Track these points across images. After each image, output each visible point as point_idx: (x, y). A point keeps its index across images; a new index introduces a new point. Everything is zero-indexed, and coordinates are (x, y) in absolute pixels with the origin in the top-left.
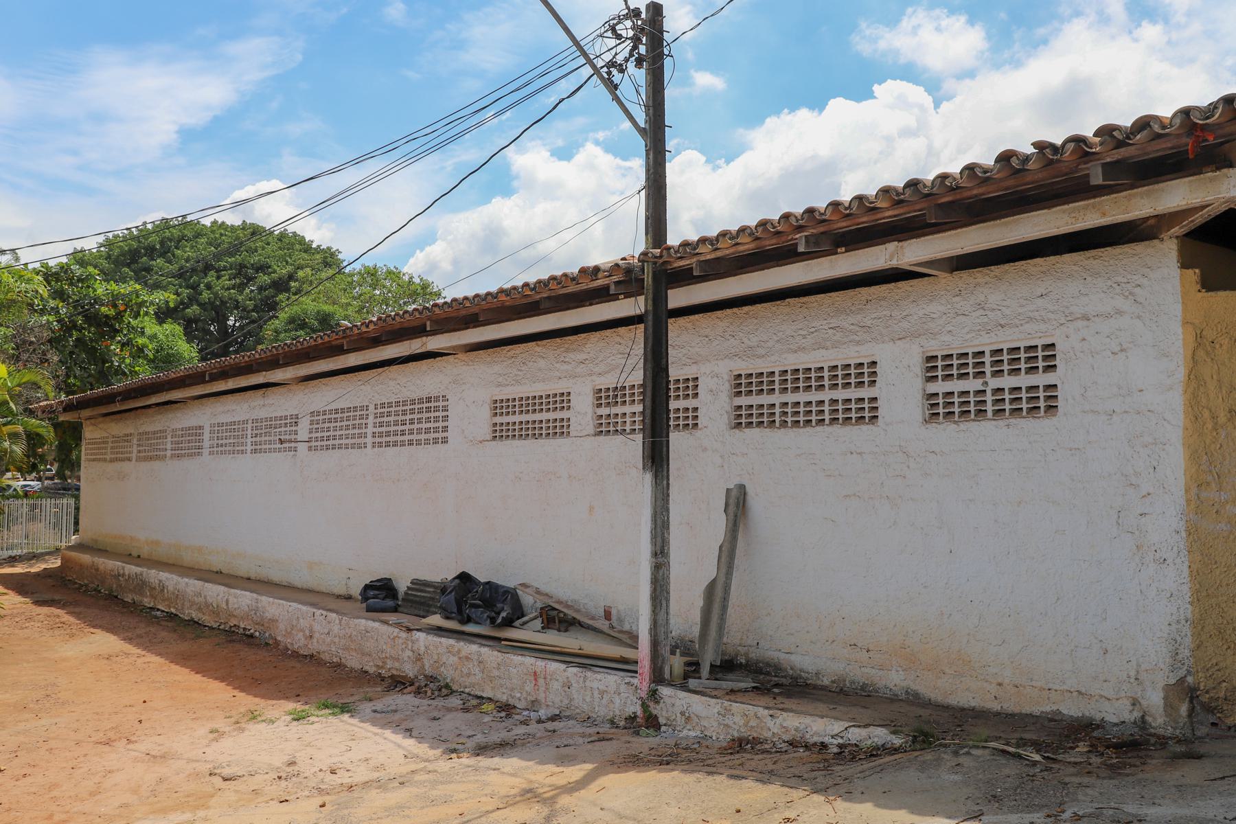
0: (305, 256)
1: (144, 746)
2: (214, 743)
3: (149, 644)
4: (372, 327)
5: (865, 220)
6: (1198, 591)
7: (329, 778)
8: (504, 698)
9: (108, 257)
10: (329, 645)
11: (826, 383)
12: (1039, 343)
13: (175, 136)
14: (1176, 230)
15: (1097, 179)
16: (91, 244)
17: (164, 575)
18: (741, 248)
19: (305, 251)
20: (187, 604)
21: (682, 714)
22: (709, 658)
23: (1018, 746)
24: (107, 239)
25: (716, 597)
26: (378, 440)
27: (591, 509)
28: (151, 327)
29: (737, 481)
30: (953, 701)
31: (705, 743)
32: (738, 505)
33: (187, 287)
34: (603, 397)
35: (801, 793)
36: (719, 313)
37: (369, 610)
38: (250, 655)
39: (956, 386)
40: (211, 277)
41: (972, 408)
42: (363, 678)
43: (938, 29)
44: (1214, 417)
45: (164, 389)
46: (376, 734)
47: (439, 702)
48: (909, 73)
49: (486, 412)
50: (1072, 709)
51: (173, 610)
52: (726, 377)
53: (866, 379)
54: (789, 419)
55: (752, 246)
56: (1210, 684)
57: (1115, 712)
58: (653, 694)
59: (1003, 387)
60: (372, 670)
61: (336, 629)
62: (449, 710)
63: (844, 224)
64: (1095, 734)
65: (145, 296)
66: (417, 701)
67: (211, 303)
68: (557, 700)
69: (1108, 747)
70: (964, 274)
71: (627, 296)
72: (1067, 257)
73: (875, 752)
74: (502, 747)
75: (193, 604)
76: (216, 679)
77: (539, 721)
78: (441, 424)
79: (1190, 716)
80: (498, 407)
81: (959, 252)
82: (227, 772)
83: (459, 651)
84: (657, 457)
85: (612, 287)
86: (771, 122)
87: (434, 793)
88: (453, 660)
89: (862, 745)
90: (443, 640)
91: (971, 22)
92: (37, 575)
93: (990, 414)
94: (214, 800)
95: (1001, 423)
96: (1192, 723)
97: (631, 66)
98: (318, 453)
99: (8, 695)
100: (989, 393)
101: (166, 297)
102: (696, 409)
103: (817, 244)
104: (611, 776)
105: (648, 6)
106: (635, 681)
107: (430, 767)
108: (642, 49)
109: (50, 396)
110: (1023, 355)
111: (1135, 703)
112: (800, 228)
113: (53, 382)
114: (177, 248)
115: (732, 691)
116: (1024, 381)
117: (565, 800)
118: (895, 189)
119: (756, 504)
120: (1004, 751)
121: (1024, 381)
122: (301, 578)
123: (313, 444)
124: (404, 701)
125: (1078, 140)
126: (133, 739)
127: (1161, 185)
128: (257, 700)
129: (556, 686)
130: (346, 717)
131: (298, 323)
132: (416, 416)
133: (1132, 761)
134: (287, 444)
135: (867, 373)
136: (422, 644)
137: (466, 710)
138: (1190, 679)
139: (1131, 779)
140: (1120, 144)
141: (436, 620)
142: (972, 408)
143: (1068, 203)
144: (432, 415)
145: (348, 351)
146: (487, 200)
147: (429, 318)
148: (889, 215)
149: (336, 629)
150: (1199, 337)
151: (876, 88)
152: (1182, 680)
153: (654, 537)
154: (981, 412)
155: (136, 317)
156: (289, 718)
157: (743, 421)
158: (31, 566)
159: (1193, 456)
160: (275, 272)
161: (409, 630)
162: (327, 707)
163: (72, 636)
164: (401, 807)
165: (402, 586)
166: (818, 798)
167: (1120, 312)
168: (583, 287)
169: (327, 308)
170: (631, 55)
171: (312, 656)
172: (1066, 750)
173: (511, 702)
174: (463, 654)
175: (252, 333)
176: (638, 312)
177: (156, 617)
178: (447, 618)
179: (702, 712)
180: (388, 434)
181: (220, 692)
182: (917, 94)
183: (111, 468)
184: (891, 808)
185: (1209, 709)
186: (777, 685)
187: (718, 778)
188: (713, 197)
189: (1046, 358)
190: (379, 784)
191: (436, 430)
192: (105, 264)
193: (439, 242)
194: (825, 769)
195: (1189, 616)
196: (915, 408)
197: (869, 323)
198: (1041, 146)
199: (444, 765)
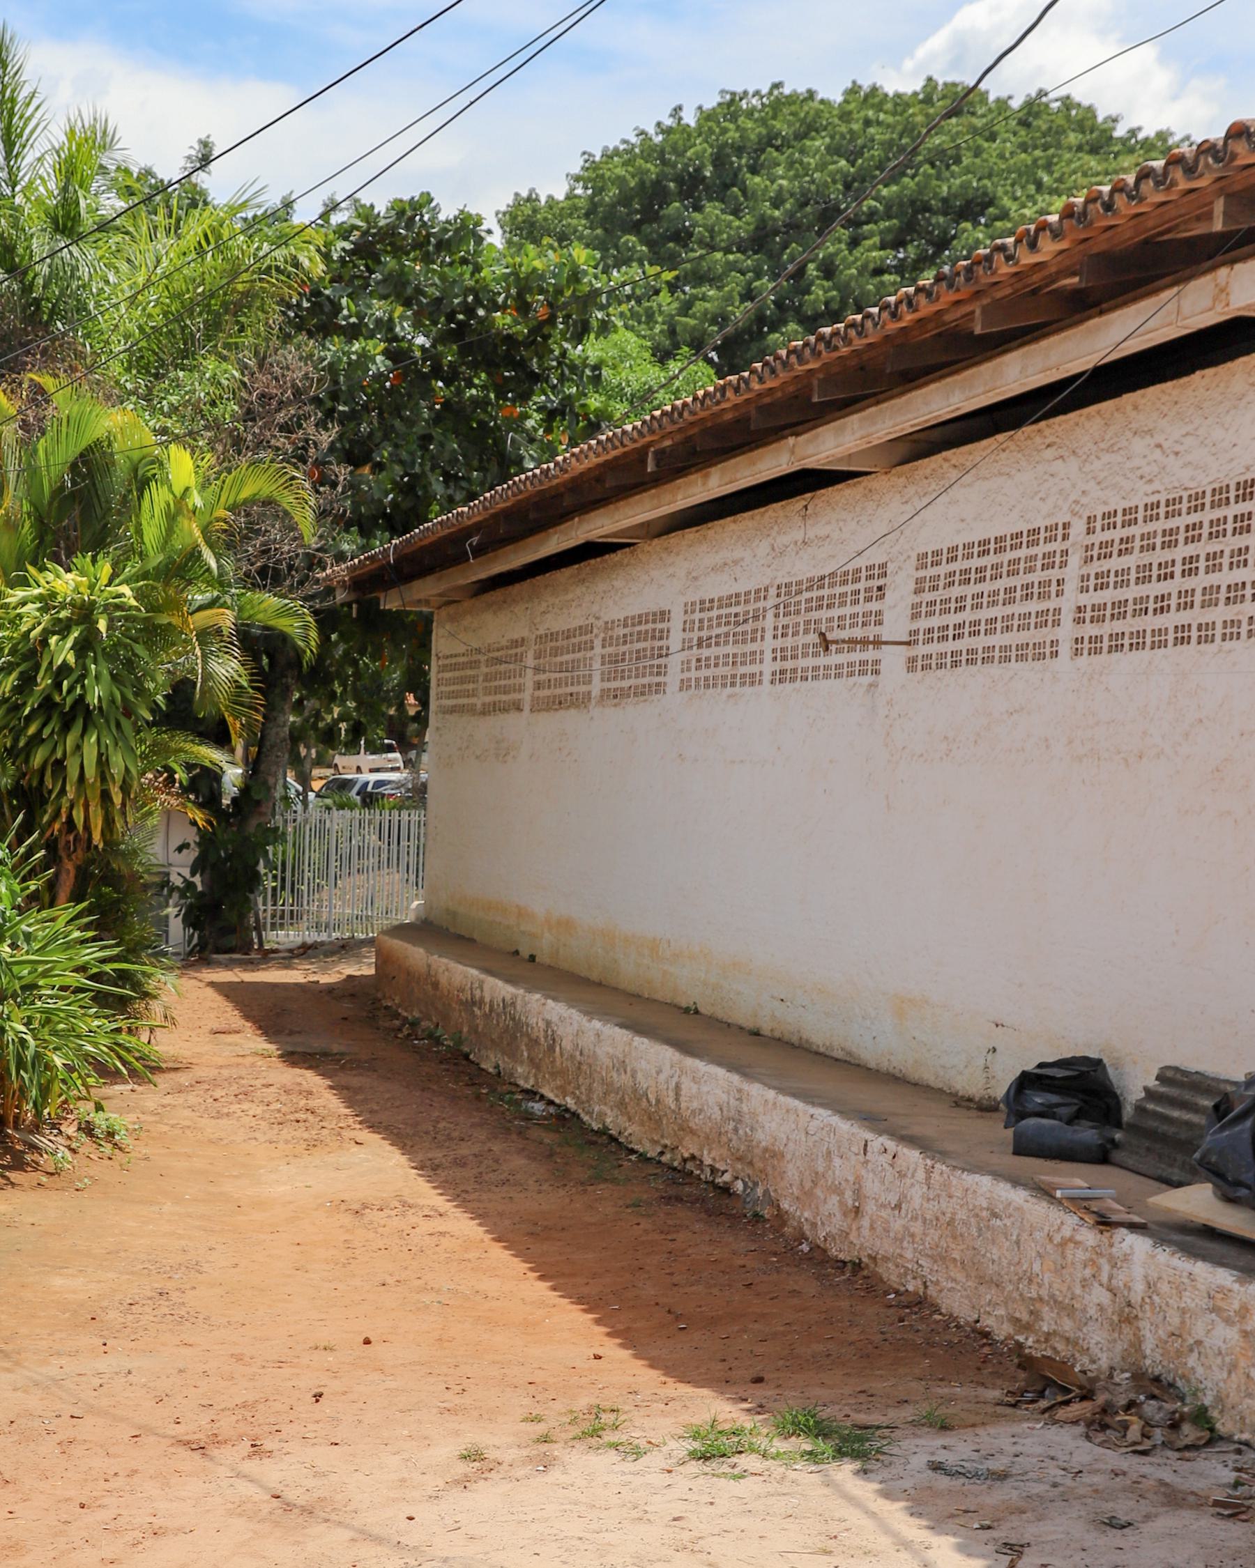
1: (272, 1472)
2: (456, 1492)
10: (899, 1240)
19: (1094, 150)
20: (598, 1089)
26: (1090, 630)
37: (1022, 1148)
40: (833, 245)
46: (905, 1545)
47: (1161, 1469)
51: (570, 1102)
60: (1002, 1331)
61: (916, 1194)
62: (1174, 1499)
75: (609, 1088)
76: (580, 1300)
88: (1225, 1336)
90: (1201, 1269)
92: (330, 990)
98: (932, 676)
114: (754, 170)
122: (878, 1041)
123: (921, 650)
124: (1046, 1444)
126: (268, 1445)
130: (844, 1471)
132: (1203, 548)
136: (1138, 1271)
141: (1197, 1201)
149: (916, 1194)
155: (580, 333)
158: (324, 970)
160: (1004, 216)
161: (1105, 1223)
163: (312, 1145)
165: (1134, 1082)
171: (857, 1266)
177: (528, 1117)
178: (1230, 1200)
180: (1120, 610)
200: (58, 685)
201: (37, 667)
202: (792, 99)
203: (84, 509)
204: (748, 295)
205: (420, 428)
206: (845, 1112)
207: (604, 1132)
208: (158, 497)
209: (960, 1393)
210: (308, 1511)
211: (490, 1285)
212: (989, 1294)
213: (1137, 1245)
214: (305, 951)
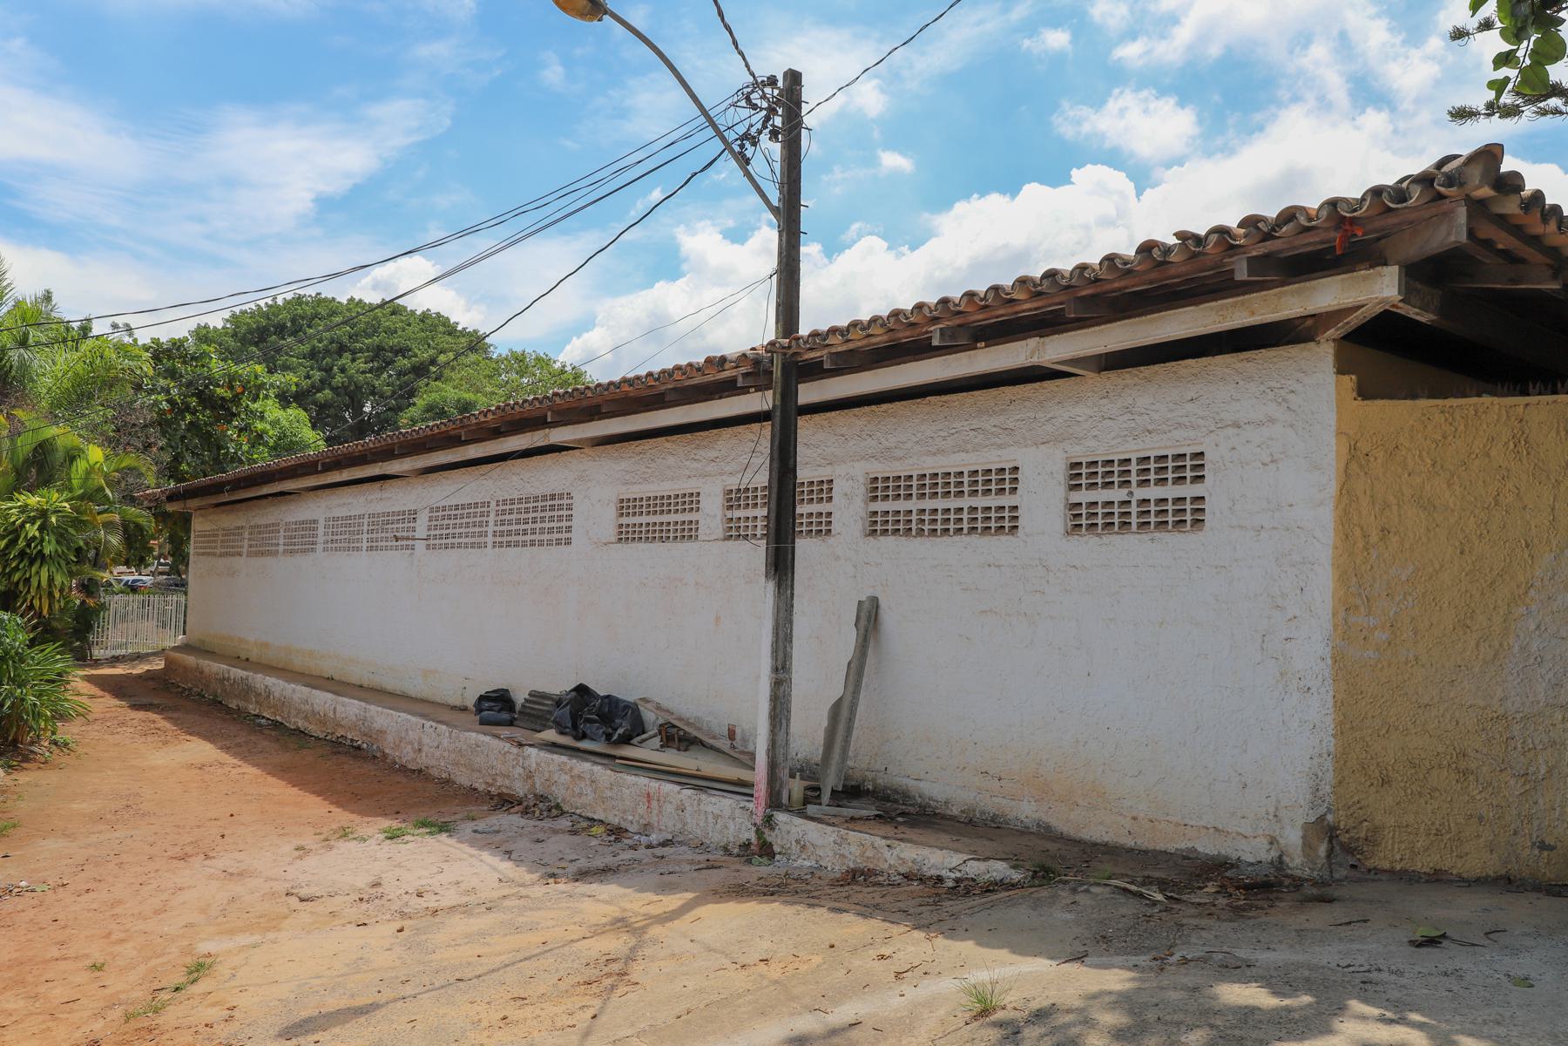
0: (449, 339)
1: (220, 863)
3: (245, 753)
4: (490, 416)
5: (1003, 313)
6: (1341, 723)
7: (416, 903)
8: (615, 820)
9: (235, 335)
11: (966, 489)
12: (1188, 451)
13: (311, 205)
14: (1332, 333)
15: (1242, 274)
16: (217, 321)
17: (270, 681)
18: (874, 340)
21: (798, 842)
22: (831, 782)
23: (1143, 884)
24: (234, 315)
25: (841, 716)
26: (498, 539)
27: (718, 619)
28: (272, 410)
29: (869, 593)
30: (1086, 835)
31: (818, 874)
32: (870, 618)
33: (320, 369)
34: (733, 499)
35: (902, 929)
36: (856, 410)
38: (352, 768)
39: (1101, 495)
40: (345, 359)
41: (1116, 520)
42: (471, 795)
43: (1146, 111)
44: (1365, 536)
45: (286, 477)
47: (547, 824)
48: (1114, 158)
49: (612, 512)
50: (1208, 847)
52: (862, 480)
53: (1007, 486)
54: (926, 527)
55: (885, 338)
56: (1351, 823)
57: (1252, 851)
58: (769, 821)
59: (1147, 498)
60: (481, 787)
61: (445, 742)
62: (555, 832)
63: (980, 317)
64: (1228, 874)
65: (266, 379)
66: (523, 822)
67: (345, 388)
68: (670, 824)
69: (1238, 888)
70: (1112, 374)
71: (759, 389)
72: (1220, 359)
73: (991, 887)
74: (605, 873)
75: (299, 711)
77: (649, 847)
78: (564, 524)
79: (1328, 857)
80: (626, 507)
81: (1102, 350)
82: (304, 892)
83: (571, 769)
84: (781, 565)
85: (740, 379)
86: (960, 207)
87: (521, 919)
88: (565, 778)
89: (980, 880)
91: (1181, 104)
92: (139, 676)
93: (1134, 526)
94: (288, 921)
95: (1145, 537)
96: (1330, 864)
97: (764, 138)
98: (436, 552)
99: (85, 805)
100: (1134, 504)
101: (291, 379)
102: (829, 514)
103: (953, 337)
104: (710, 906)
105: (785, 74)
106: (751, 806)
107: (523, 891)
108: (778, 121)
109: (152, 483)
110: (1170, 464)
111: (1273, 841)
112: (935, 320)
113: (154, 468)
114: (309, 326)
115: (852, 819)
116: (1170, 491)
117: (656, 931)
118: (1032, 280)
119: (888, 618)
120: (1125, 890)
121: (1170, 491)
122: (416, 687)
124: (510, 821)
125: (1222, 231)
127: (1314, 283)
128: (353, 816)
129: (669, 808)
130: (444, 836)
131: (435, 411)
132: (539, 515)
133: (1260, 903)
134: (403, 541)
135: (1007, 479)
137: (574, 832)
138: (1330, 817)
139: (1251, 922)
140: (1267, 237)
141: (550, 735)
142: (1116, 520)
143: (1216, 300)
144: (556, 513)
145: (467, 442)
146: (650, 285)
147: (550, 408)
148: (1027, 307)
149: (445, 742)
150: (1353, 448)
151: (1074, 172)
152: (1322, 818)
153: (775, 651)
154: (1125, 525)
155: (255, 399)
156: (382, 836)
157: (879, 528)
159: (1342, 577)
161: (520, 745)
162: (424, 825)
163: (165, 743)
164: (482, 934)
165: (520, 697)
166: (919, 935)
167: (1272, 420)
168: (710, 378)
169: (469, 396)
170: (764, 127)
171: (420, 771)
172: (1193, 890)
173: (623, 825)
174: (576, 772)
175: (385, 421)
176: (765, 408)
178: (562, 733)
179: (818, 841)
180: (509, 533)
181: (315, 806)
182: (1119, 180)
183: (222, 562)
184: (993, 947)
185: (1348, 850)
186: (903, 814)
187: (819, 911)
188: (858, 282)
189: (1194, 468)
190: (464, 909)
191: (559, 530)
192: (231, 343)
193: (597, 329)
194: (935, 904)
195: (1332, 749)
196: (1057, 519)
197: (1011, 426)
198: (1182, 236)
199: (538, 891)
200: (29, 545)
201: (18, 538)
202: (325, 300)
203: (41, 466)
204: (308, 377)
205: (181, 432)
206: (413, 714)
207: (298, 729)
208: (80, 466)
209: (474, 809)
210: (240, 874)
211: (274, 791)
212: (476, 775)
213: (533, 751)
214: (115, 660)
